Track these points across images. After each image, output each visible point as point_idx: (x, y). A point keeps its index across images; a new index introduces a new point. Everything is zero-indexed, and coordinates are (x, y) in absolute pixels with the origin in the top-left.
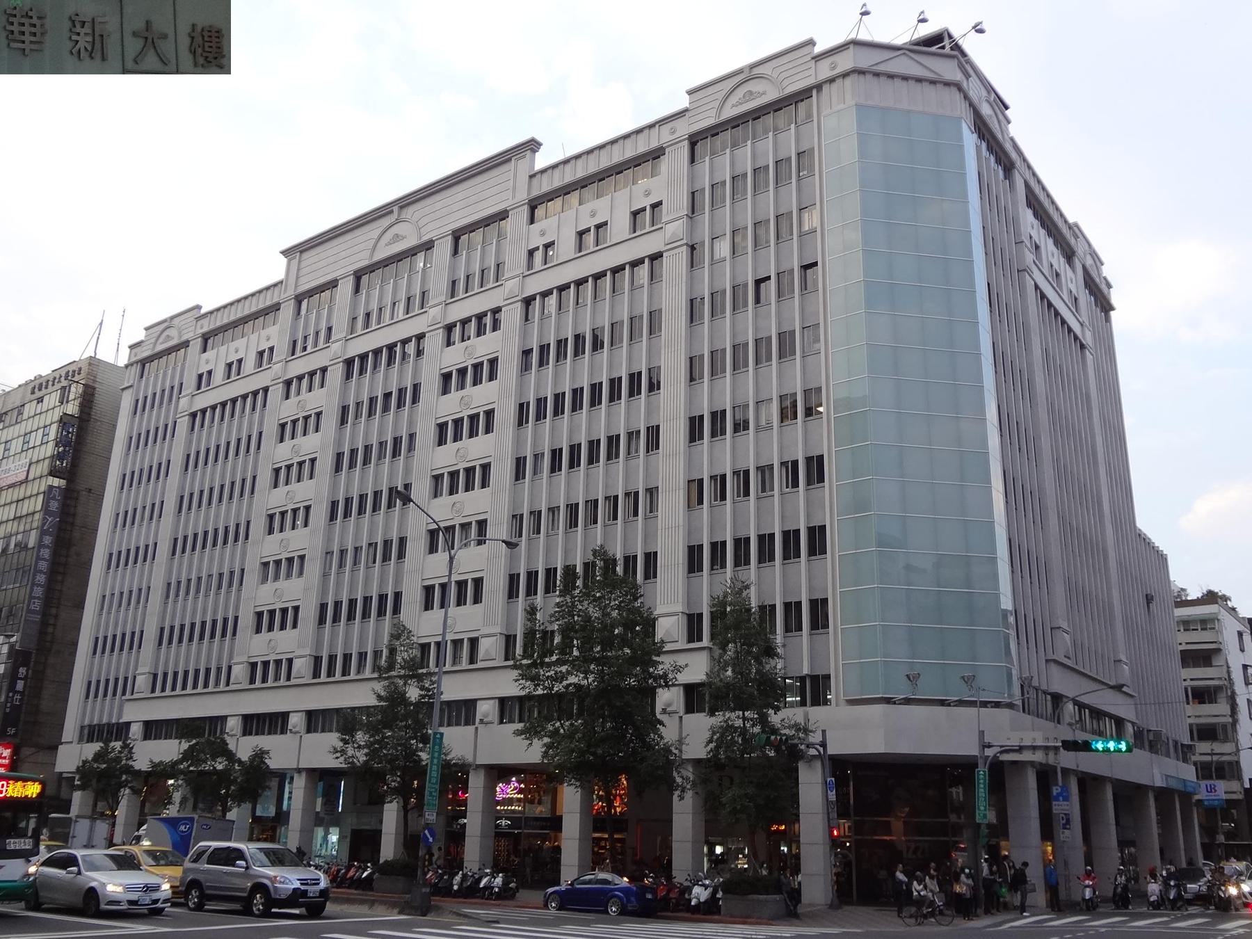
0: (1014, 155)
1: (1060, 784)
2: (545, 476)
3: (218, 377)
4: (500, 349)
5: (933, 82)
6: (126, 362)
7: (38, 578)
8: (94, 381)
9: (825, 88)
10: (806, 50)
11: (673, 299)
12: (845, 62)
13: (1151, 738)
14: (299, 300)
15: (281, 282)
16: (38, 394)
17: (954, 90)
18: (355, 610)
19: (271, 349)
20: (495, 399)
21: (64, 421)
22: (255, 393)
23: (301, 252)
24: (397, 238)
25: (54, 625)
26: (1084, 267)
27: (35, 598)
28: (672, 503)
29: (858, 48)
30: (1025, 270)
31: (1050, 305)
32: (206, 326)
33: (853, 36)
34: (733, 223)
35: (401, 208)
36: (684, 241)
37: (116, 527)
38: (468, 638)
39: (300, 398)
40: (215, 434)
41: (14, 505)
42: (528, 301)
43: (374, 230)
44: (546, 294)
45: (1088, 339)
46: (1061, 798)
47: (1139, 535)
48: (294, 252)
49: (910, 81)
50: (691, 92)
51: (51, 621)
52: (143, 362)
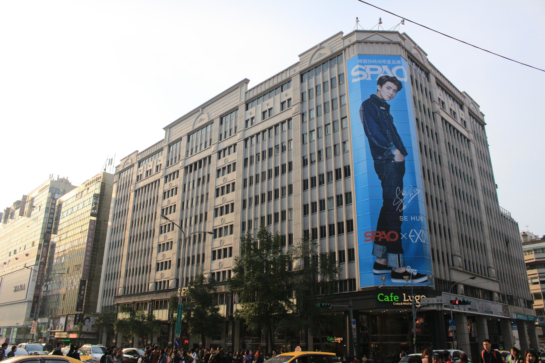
0: (429, 68)
1: (452, 319)
2: (253, 207)
3: (144, 176)
4: (236, 159)
5: (389, 43)
6: (114, 173)
7: (87, 253)
8: (105, 181)
9: (347, 49)
10: (340, 36)
11: (296, 135)
12: (354, 39)
13: (509, 298)
14: (170, 146)
15: (163, 140)
16: (88, 187)
17: (397, 45)
18: (189, 261)
19: (161, 165)
20: (235, 178)
21: (95, 196)
22: (156, 182)
23: (170, 128)
24: (201, 120)
25: (94, 270)
26: (469, 109)
27: (87, 261)
28: (297, 215)
29: (358, 33)
30: (436, 112)
31: (450, 125)
32: (140, 158)
33: (356, 29)
34: (316, 104)
35: (203, 108)
36: (299, 112)
37: (112, 234)
38: (228, 270)
39: (171, 182)
40: (144, 197)
41: (81, 227)
42: (246, 140)
43: (193, 118)
44: (252, 137)
45: (471, 137)
46: (452, 325)
47: (502, 215)
48: (168, 128)
49: (379, 44)
50: (300, 56)
51: (93, 269)
52: (120, 173)
